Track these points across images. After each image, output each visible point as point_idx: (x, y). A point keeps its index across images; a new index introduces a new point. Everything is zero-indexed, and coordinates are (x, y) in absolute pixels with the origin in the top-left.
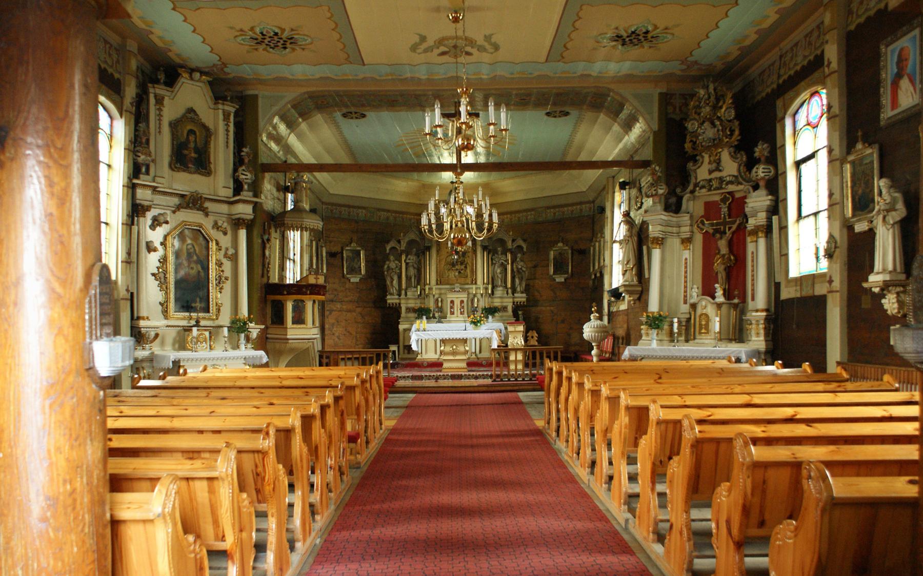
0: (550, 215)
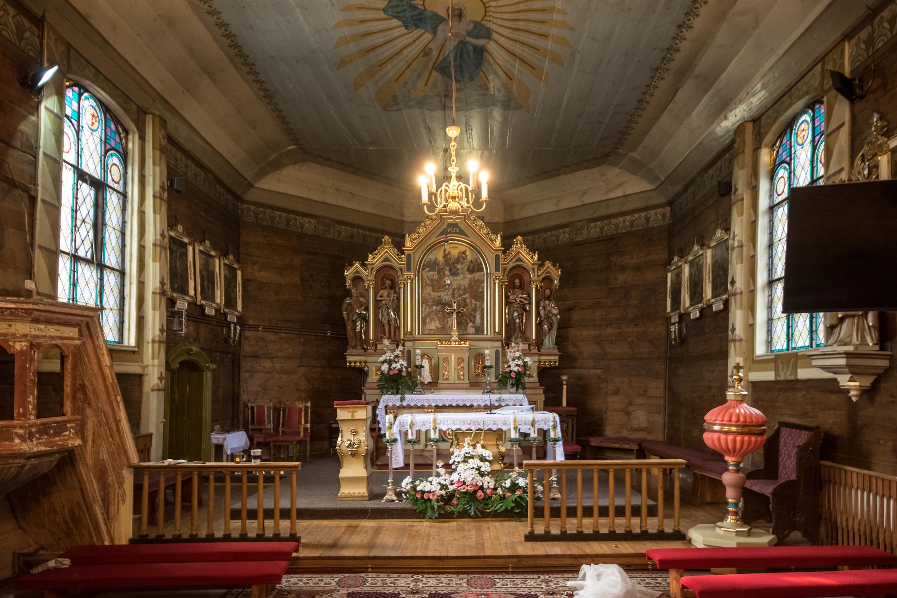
0: (594, 231)
